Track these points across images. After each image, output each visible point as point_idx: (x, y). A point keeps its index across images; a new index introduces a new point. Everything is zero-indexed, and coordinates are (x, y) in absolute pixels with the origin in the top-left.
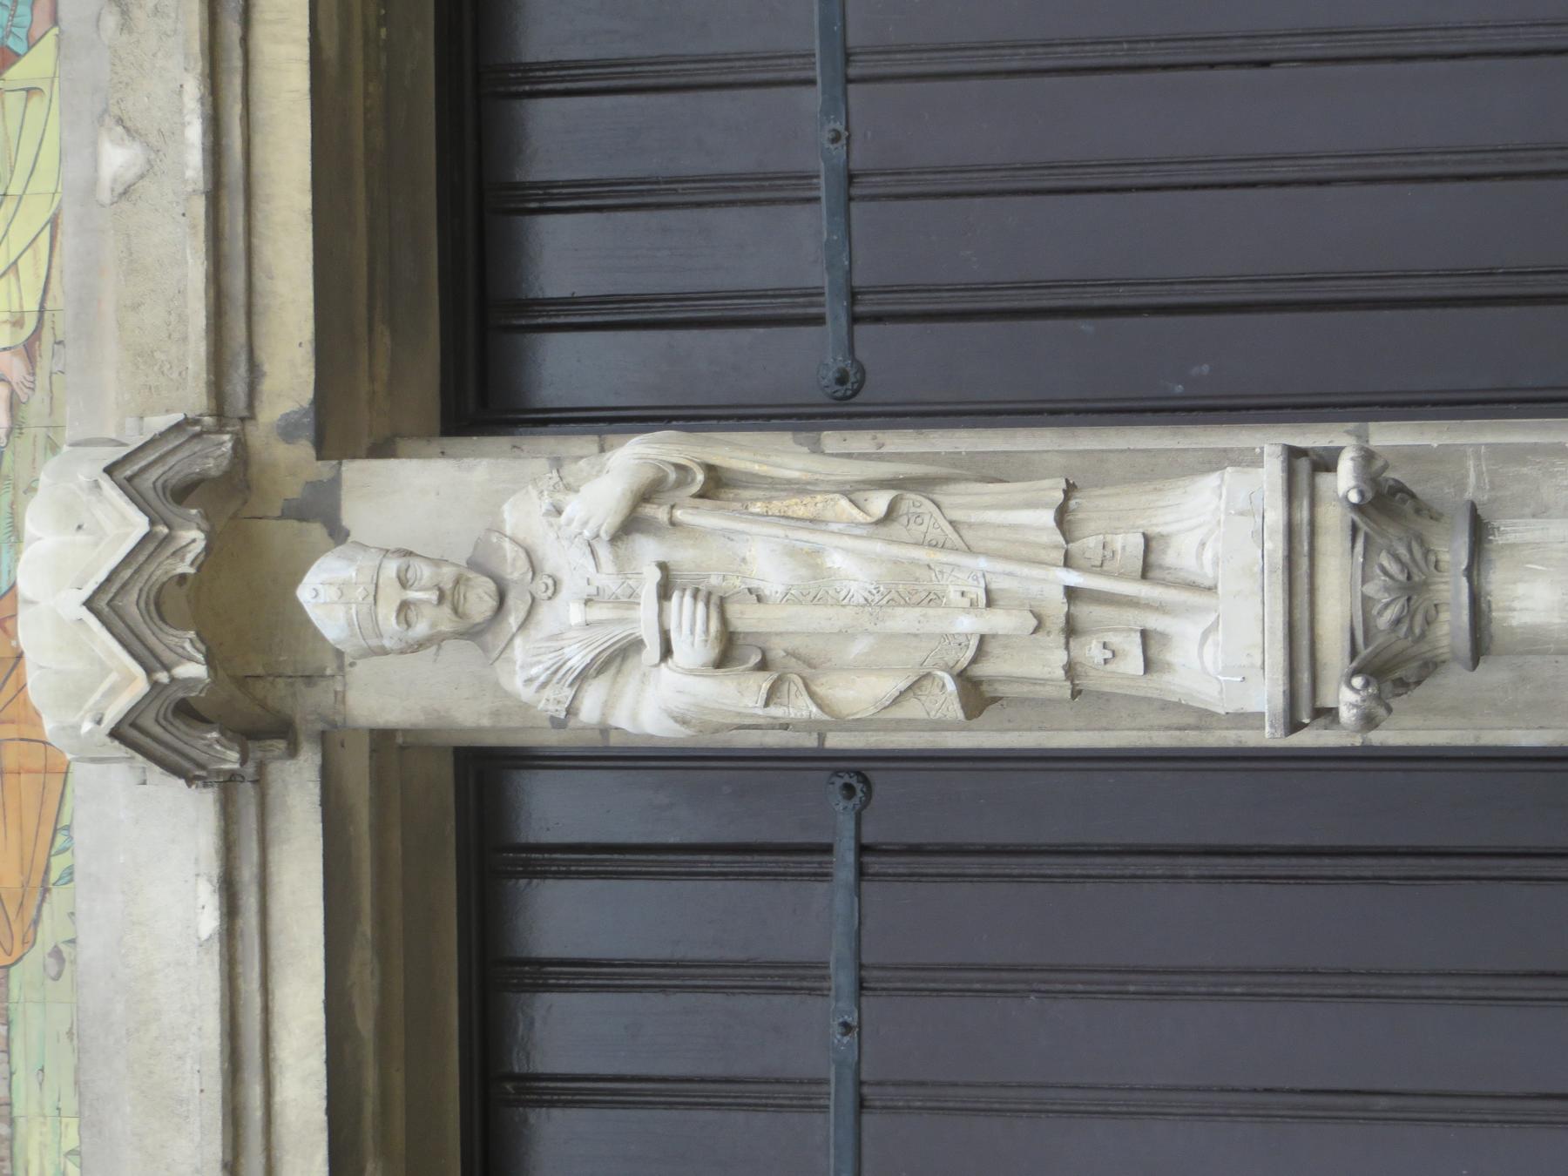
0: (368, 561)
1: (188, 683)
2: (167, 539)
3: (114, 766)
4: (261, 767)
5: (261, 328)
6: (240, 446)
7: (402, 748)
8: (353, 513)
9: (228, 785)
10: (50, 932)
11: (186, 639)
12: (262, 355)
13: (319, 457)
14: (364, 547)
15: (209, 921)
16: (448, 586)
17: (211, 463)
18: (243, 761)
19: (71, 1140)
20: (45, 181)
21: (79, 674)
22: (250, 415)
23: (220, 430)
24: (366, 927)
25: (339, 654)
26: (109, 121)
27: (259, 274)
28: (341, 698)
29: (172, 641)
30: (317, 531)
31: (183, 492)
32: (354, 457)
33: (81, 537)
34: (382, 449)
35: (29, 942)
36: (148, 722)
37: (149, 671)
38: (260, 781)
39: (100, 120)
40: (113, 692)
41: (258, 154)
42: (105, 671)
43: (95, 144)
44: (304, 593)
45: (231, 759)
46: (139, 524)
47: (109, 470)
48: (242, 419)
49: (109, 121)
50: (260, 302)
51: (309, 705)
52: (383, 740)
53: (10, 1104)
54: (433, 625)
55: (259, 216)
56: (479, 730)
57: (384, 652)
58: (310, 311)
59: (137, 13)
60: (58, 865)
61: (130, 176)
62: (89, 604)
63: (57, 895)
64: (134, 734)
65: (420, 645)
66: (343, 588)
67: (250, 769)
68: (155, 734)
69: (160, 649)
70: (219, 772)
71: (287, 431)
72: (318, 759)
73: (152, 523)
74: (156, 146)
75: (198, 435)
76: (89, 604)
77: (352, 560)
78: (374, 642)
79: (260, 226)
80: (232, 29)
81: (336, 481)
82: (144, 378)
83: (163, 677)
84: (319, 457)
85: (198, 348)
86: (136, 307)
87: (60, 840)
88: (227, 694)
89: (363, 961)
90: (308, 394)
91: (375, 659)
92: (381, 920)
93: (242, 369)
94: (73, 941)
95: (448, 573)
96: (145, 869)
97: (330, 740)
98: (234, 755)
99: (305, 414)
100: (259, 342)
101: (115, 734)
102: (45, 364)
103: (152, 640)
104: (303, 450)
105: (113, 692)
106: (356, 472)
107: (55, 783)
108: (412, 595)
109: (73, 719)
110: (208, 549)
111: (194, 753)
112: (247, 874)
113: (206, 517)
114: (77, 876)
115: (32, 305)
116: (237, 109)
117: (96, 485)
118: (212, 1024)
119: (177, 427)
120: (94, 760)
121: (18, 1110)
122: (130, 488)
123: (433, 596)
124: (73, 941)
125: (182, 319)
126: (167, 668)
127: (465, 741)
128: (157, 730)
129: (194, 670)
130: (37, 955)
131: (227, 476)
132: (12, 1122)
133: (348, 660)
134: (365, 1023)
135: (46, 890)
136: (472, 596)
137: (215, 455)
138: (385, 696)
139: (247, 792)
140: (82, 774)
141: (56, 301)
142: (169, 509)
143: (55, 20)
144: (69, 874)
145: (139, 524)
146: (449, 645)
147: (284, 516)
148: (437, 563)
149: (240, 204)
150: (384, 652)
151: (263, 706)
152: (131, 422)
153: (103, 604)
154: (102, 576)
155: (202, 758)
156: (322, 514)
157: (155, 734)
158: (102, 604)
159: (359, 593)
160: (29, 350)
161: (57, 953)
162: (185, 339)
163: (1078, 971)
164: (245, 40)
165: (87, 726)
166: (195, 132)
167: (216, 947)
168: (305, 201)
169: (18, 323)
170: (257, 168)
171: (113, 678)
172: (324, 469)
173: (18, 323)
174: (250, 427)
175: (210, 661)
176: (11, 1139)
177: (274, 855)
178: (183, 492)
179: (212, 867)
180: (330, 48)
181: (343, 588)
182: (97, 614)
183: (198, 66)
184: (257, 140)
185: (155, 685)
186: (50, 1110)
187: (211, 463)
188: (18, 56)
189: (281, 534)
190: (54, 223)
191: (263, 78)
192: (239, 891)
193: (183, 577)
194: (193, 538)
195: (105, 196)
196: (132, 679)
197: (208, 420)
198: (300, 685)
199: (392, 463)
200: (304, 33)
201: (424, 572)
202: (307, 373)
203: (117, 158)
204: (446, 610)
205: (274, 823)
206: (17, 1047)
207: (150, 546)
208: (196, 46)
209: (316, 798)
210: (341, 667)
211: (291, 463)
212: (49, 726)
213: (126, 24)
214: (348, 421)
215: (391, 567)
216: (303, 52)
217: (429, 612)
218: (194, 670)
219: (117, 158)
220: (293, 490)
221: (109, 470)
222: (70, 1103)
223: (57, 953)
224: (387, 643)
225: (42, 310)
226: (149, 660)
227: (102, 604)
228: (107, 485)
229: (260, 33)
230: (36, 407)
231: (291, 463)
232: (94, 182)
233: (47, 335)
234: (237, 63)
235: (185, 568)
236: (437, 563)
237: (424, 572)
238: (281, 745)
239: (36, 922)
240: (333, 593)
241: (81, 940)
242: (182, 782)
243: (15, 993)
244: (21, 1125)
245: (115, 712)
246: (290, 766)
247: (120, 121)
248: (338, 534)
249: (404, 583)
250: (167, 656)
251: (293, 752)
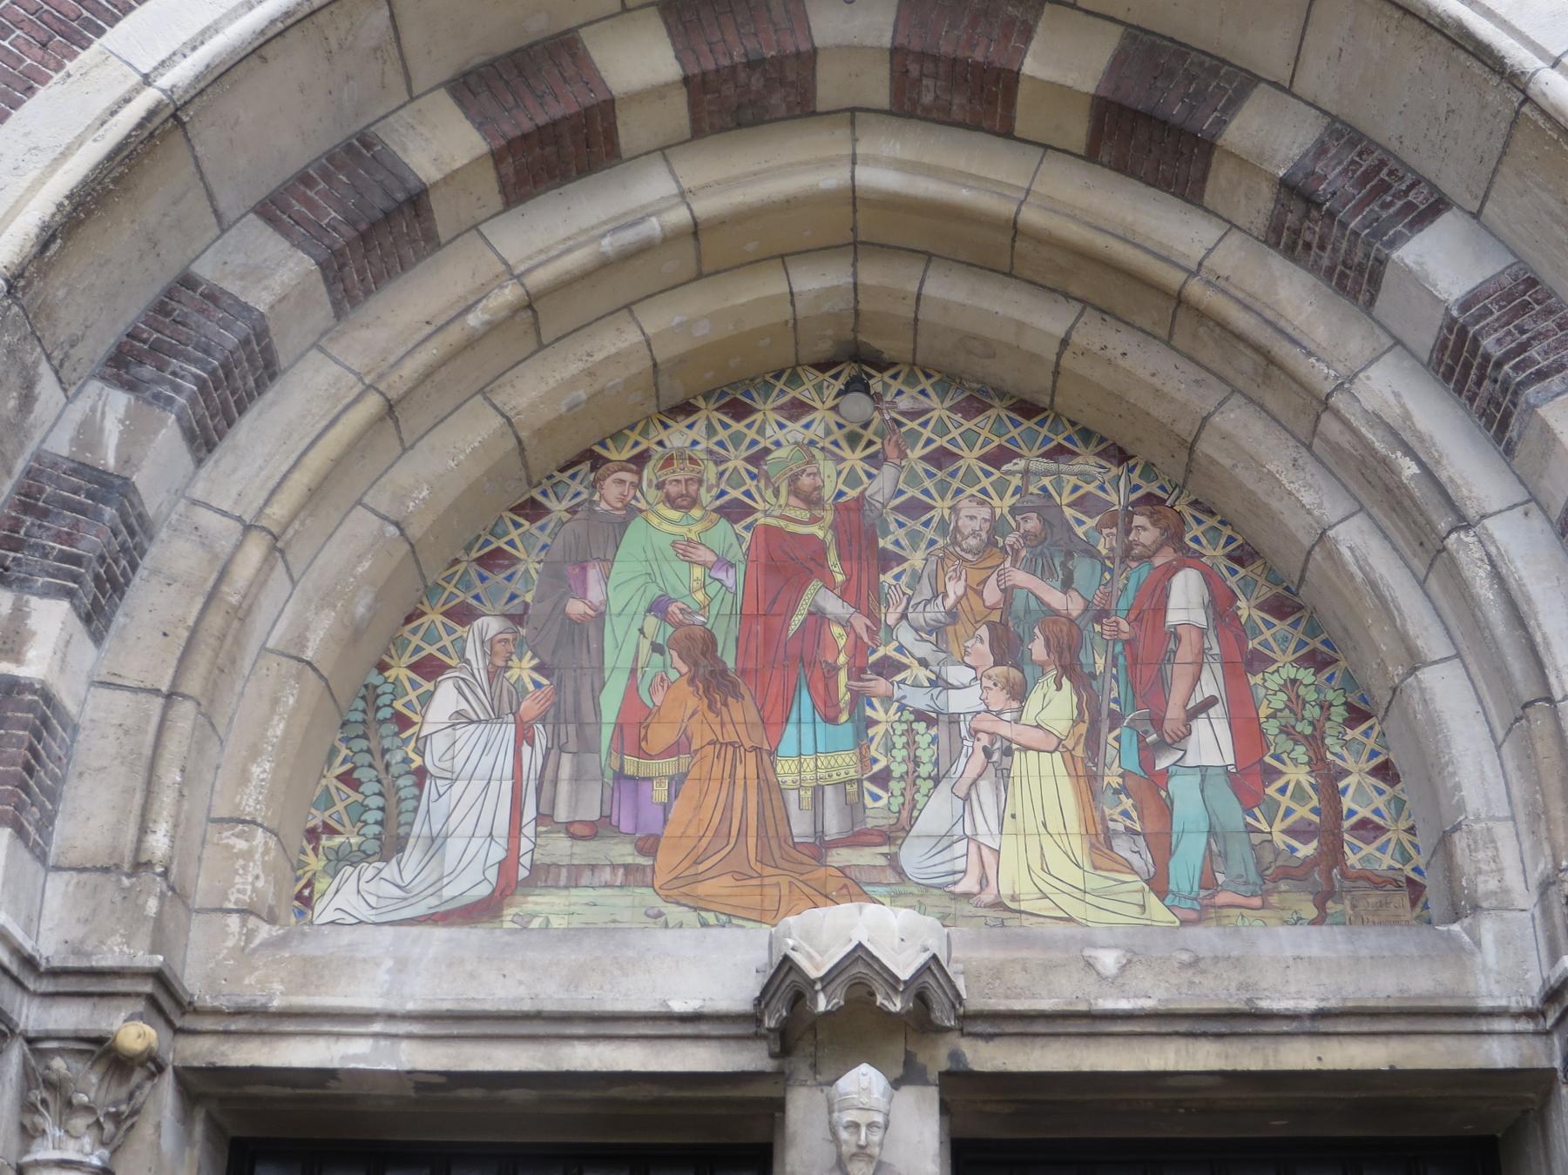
0: (882, 1104)
1: (815, 1001)
2: (895, 990)
3: (766, 954)
4: (764, 1037)
5: (1014, 1042)
6: (949, 1030)
7: (772, 1116)
8: (908, 1094)
9: (754, 1018)
10: (674, 912)
11: (839, 1001)
12: (997, 1041)
13: (941, 1074)
14: (890, 1102)
15: (678, 1006)
16: (868, 1151)
17: (938, 1014)
18: (769, 1030)
19: (557, 922)
20: (1092, 914)
21: (823, 936)
22: (963, 1034)
23: (957, 1017)
24: (671, 1093)
25: (831, 1083)
26: (1129, 955)
27: (1045, 1040)
28: (803, 1084)
29: (838, 992)
30: (898, 1071)
31: (922, 998)
32: (941, 1093)
33: (897, 940)
34: (945, 1108)
35: (667, 899)
36: (792, 977)
37: (821, 979)
38: (756, 1037)
39: (1129, 950)
40: (810, 957)
41: (1111, 1040)
42: (821, 954)
43: (1116, 947)
44: (864, 1068)
45: (770, 1023)
46: (904, 975)
47: (934, 957)
48: (961, 1030)
49: (1129, 955)
50: (1028, 1041)
51: (802, 1069)
52: (779, 1105)
53: (576, 886)
54: (846, 1142)
55: (1077, 1040)
56: (783, 1165)
57: (831, 1112)
58: (1024, 1069)
59: (1190, 973)
60: (710, 918)
61: (1099, 967)
62: (860, 946)
63: (691, 917)
64: (786, 968)
65: (834, 1133)
66: (867, 1090)
67: (763, 1031)
68: (784, 977)
69: (834, 985)
70: (763, 1014)
71: (955, 1056)
72: (768, 1069)
73: (905, 982)
74: (1113, 983)
75: (954, 1006)
76: (860, 946)
77: (883, 1095)
78: (836, 1107)
79: (1071, 1041)
80: (1183, 1027)
81: (926, 1083)
82: (984, 974)
83: (818, 986)
84: (941, 1074)
85: (1002, 1005)
86: (1025, 970)
87: (723, 918)
88: (809, 1022)
89: (655, 1092)
90: (977, 1068)
91: (825, 1104)
92: (673, 1102)
93: (991, 1030)
94: (666, 926)
95: (876, 1151)
96: (708, 969)
97: (780, 1077)
98: (773, 1024)
99: (965, 1065)
100: (1006, 1039)
101: (786, 958)
102: (991, 913)
103: (839, 980)
104: (945, 1065)
105: (810, 957)
106: (932, 1094)
107: (754, 915)
108: (863, 1130)
109: (794, 934)
110: (890, 1013)
111: (774, 1001)
112: (704, 1028)
113: (908, 1012)
114: (704, 930)
115: (1024, 906)
116: (1138, 1029)
117: (926, 950)
118: (620, 1006)
119: (958, 996)
120: (770, 944)
121: (574, 891)
122: (925, 969)
123: (862, 1142)
124: (666, 926)
125: (1018, 996)
126: (823, 989)
127: (776, 1151)
128: (788, 982)
129: (822, 1004)
130: (659, 903)
131: (931, 1022)
132: (566, 887)
133: (826, 1089)
134: (616, 1092)
135: (695, 909)
136: (862, 1165)
137: (942, 1015)
138: (804, 1110)
139: (751, 1029)
140: (763, 932)
141: (1027, 921)
142: (913, 991)
143: (1184, 922)
144: (705, 924)
145: (904, 975)
146: (833, 1148)
147: (907, 1052)
148: (881, 1145)
149: (1084, 1030)
150: (831, 1112)
151: (800, 1039)
152: (960, 967)
153: (859, 954)
154: (876, 953)
155: (772, 1006)
156: (907, 1076)
157: (784, 977)
158: (860, 953)
159: (865, 1100)
160: (998, 905)
161: (660, 915)
162: (1007, 997)
163: (127, 101)
164: (1177, 1034)
165: (791, 942)
166: (1124, 1005)
167: (663, 1010)
168: (1085, 1068)
169: (1014, 898)
170: (1104, 1040)
171: (818, 958)
172: (933, 1076)
173: (1014, 898)
174: (957, 1034)
175: (827, 1013)
176: (557, 887)
177: (714, 1044)
178: (922, 998)
179: (710, 1007)
180: (1171, 1082)
181: (867, 1090)
182: (854, 950)
183: (1162, 1007)
184: (1121, 1040)
185: (814, 982)
186: (572, 909)
187: (938, 1014)
188: (1162, 900)
189: (897, 1050)
190: (1070, 919)
191: (1155, 1044)
192: (694, 1026)
193: (872, 994)
194: (896, 1005)
195: (1087, 952)
196: (817, 968)
197: (961, 1010)
198: (810, 1060)
199: (937, 1116)
200: (1182, 1067)
201: (876, 1137)
202: (988, 1067)
203: (1108, 960)
204: (854, 1150)
205: (732, 1044)
206: (609, 891)
207: (892, 981)
208: (1173, 1006)
209: (746, 1068)
210: (820, 1084)
211: (937, 1058)
212: (791, 920)
213: (1184, 966)
214: (962, 1093)
215: (879, 1118)
216: (1171, 1067)
217: (853, 1139)
218: (822, 1004)
219: (1108, 960)
220: (922, 1058)
221: (934, 957)
222: (576, 922)
223: (660, 915)
224: (836, 1115)
225: (1021, 912)
226: (828, 979)
227: (860, 953)
228: (924, 957)
229: (1181, 1043)
230: (968, 909)
231: (937, 1058)
232: (1094, 946)
233: (1006, 915)
234: (1164, 1029)
235: (880, 1000)
236: (881, 1145)
237: (876, 1137)
238: (777, 1049)
239: (678, 903)
240: (864, 1084)
241: (669, 932)
242: (757, 994)
243: (639, 890)
244: (564, 893)
245: (798, 958)
246: (765, 1053)
247: (1129, 961)
248: (896, 1084)
249: (870, 1125)
250: (830, 989)
251: (773, 1056)
